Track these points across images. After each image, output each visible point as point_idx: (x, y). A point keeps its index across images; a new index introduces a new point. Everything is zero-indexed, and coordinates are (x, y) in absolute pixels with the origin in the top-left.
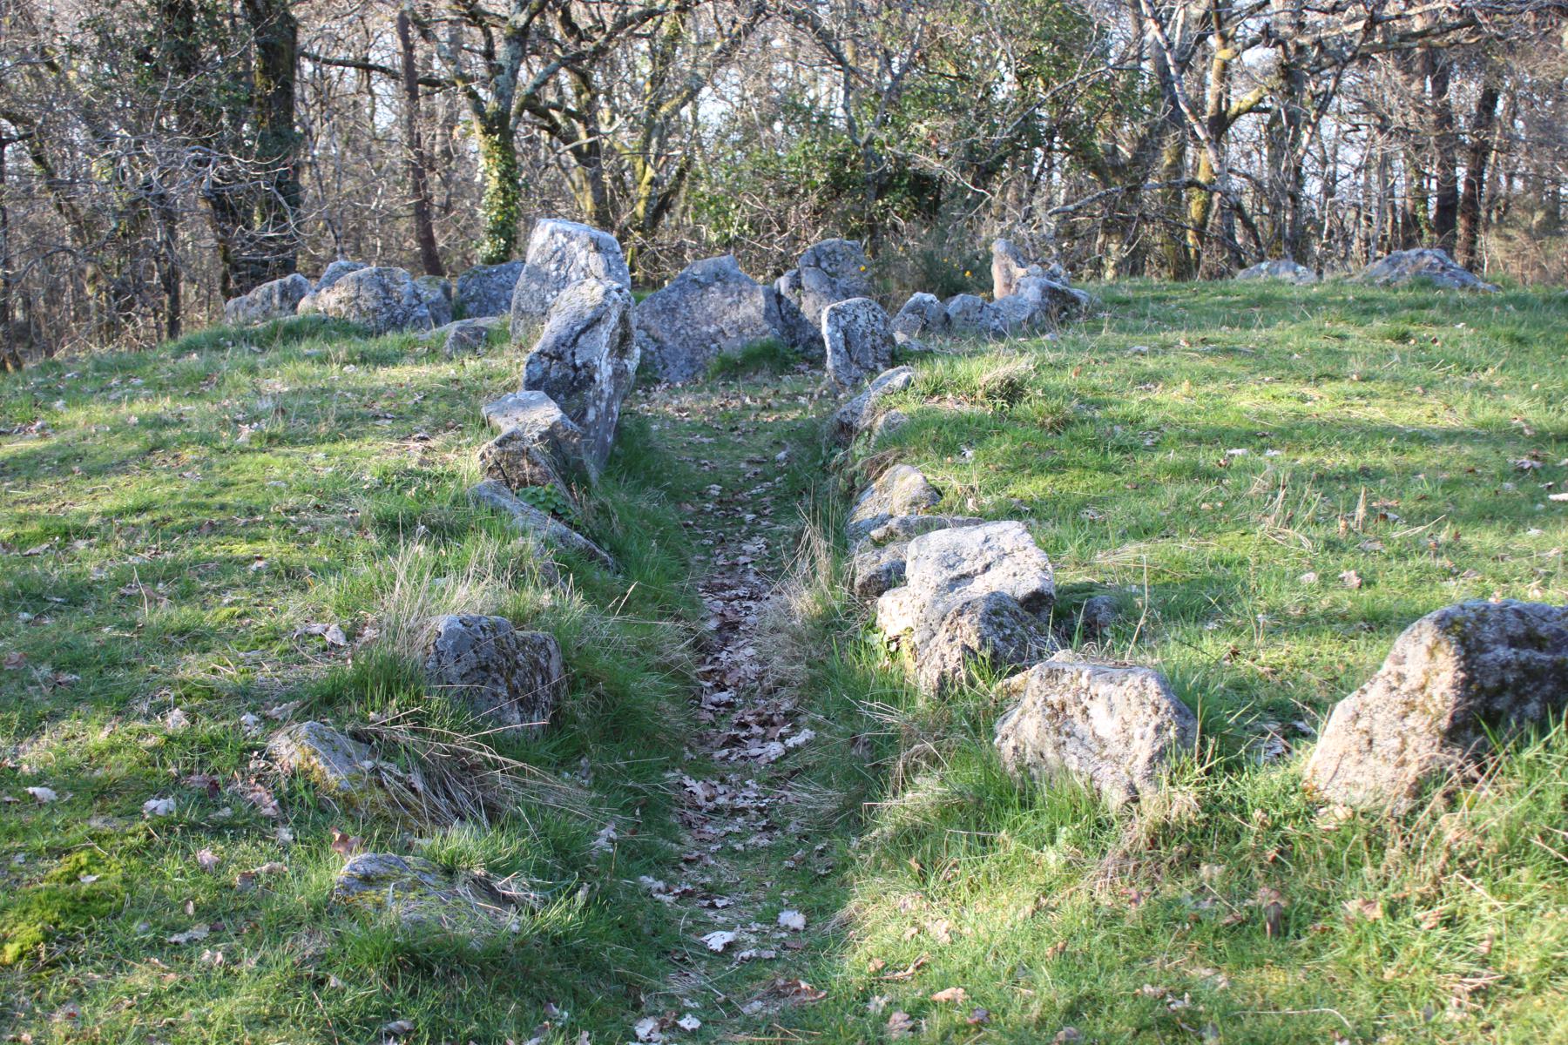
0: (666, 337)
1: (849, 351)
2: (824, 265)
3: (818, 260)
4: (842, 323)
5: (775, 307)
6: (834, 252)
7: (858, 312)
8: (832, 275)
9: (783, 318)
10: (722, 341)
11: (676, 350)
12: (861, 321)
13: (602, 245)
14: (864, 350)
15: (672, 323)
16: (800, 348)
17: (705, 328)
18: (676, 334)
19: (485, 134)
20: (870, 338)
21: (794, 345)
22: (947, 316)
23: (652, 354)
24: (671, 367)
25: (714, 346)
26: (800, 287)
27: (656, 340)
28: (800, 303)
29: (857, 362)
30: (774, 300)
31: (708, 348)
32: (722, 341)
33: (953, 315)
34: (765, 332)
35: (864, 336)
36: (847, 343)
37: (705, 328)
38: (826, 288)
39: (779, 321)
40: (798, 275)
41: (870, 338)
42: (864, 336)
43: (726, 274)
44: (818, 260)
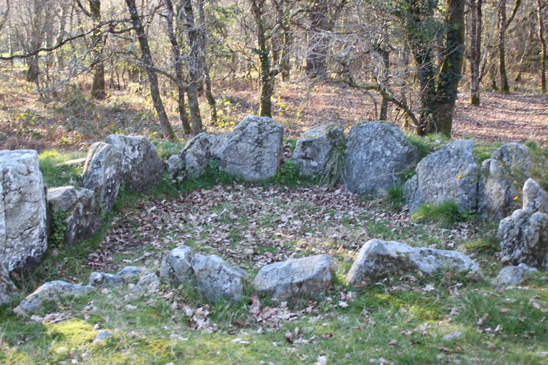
2: (505, 159)
18: (425, 183)
25: (435, 196)
44: (502, 155)
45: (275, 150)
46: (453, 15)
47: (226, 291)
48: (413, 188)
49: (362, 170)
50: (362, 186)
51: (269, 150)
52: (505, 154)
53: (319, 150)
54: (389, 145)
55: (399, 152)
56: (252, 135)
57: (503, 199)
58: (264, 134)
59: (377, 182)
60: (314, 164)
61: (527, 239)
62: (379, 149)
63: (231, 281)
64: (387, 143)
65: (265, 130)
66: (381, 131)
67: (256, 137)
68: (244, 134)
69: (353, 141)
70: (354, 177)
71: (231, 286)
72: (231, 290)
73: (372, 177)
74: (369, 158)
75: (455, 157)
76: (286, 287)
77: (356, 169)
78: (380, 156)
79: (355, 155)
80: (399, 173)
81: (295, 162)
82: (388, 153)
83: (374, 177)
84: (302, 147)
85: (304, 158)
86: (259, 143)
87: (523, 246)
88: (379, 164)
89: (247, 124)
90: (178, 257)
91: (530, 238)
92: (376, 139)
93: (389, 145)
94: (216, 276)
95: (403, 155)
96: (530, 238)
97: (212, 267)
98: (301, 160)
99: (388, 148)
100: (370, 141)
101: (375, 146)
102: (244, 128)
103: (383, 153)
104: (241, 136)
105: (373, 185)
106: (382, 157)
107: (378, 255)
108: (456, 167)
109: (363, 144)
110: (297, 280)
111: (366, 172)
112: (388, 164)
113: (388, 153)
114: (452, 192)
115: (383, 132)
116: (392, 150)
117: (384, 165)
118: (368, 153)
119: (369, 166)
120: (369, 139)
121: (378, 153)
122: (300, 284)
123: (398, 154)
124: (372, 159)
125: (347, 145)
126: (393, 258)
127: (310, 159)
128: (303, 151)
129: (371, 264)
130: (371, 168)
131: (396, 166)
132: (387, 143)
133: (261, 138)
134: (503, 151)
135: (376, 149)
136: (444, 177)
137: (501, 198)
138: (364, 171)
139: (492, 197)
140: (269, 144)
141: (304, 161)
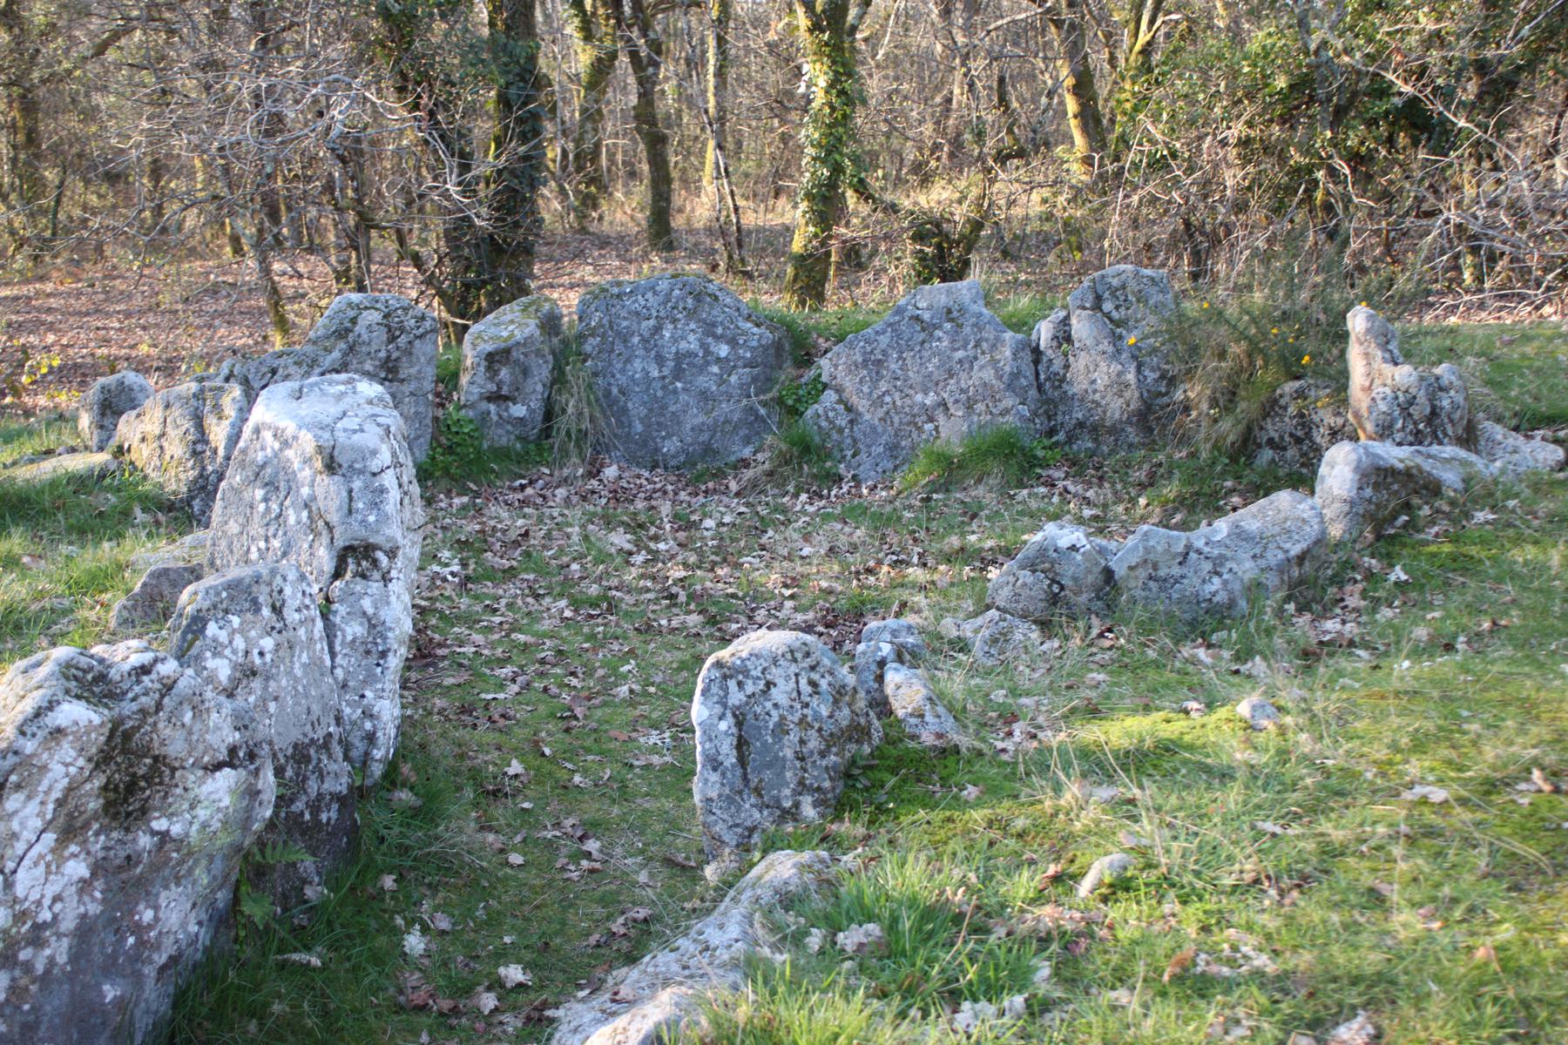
0: (862, 405)
1: (742, 761)
2: (1108, 306)
3: (1099, 299)
4: (736, 697)
5: (1029, 371)
6: (1124, 287)
7: (776, 674)
8: (1118, 324)
9: (1040, 388)
10: (941, 419)
11: (873, 428)
12: (780, 695)
13: (343, 459)
14: (777, 763)
15: (875, 384)
16: (1061, 436)
17: (919, 397)
18: (878, 402)
19: (811, 31)
20: (793, 737)
21: (1051, 432)
22: (1108, 574)
23: (841, 430)
24: (863, 456)
25: (929, 426)
26: (1068, 339)
27: (849, 409)
28: (1067, 367)
29: (758, 792)
30: (1027, 356)
31: (920, 429)
32: (941, 419)
33: (1120, 571)
34: (1006, 412)
35: (781, 729)
36: (741, 745)
37: (919, 397)
38: (1106, 345)
39: (1033, 393)
40: (1066, 321)
41: (793, 737)
42: (781, 729)
43: (962, 310)
44: (1099, 299)
45: (428, 385)
46: (512, 17)
47: (1215, 600)
48: (842, 422)
49: (658, 406)
50: (670, 446)
51: (413, 386)
52: (1106, 295)
53: (526, 372)
54: (719, 331)
55: (755, 344)
56: (374, 347)
57: (1137, 395)
58: (403, 340)
59: (713, 430)
60: (519, 410)
61: (1451, 421)
62: (691, 343)
63: (1218, 574)
64: (714, 325)
65: (403, 330)
66: (683, 299)
67: (383, 354)
68: (351, 348)
69: (603, 336)
70: (639, 427)
71: (1225, 583)
72: (1231, 592)
73: (694, 418)
74: (666, 372)
75: (948, 326)
76: (1282, 569)
77: (636, 408)
78: (698, 361)
79: (623, 371)
80: (768, 396)
81: (471, 413)
82: (723, 350)
83: (702, 418)
84: (488, 368)
85: (496, 397)
86: (389, 371)
87: (1446, 435)
88: (706, 382)
89: (354, 321)
90: (1073, 548)
91: (1457, 416)
92: (674, 321)
93: (719, 331)
94: (1176, 571)
95: (765, 348)
96: (1457, 416)
97: (1167, 551)
98: (484, 405)
99: (718, 338)
100: (658, 329)
101: (675, 340)
102: (348, 330)
103: (707, 352)
104: (345, 355)
105: (704, 437)
106: (708, 363)
107: (1378, 469)
108: (965, 347)
109: (636, 340)
110: (1295, 550)
111: (672, 408)
112: (733, 379)
113: (723, 350)
114: (980, 407)
115: (690, 301)
116: (733, 342)
117: (722, 382)
118: (660, 360)
119: (675, 391)
120: (652, 322)
121: (691, 354)
122: (1301, 559)
123: (753, 349)
124: (678, 373)
125: (588, 348)
126: (1400, 472)
127: (506, 398)
128: (491, 379)
129: (1368, 492)
130: (683, 397)
131: (755, 379)
132: (714, 325)
133: (394, 356)
134: (1100, 289)
135: (683, 345)
136: (935, 377)
137: (1127, 394)
138: (664, 407)
139: (1097, 397)
140: (413, 371)
141: (492, 407)
